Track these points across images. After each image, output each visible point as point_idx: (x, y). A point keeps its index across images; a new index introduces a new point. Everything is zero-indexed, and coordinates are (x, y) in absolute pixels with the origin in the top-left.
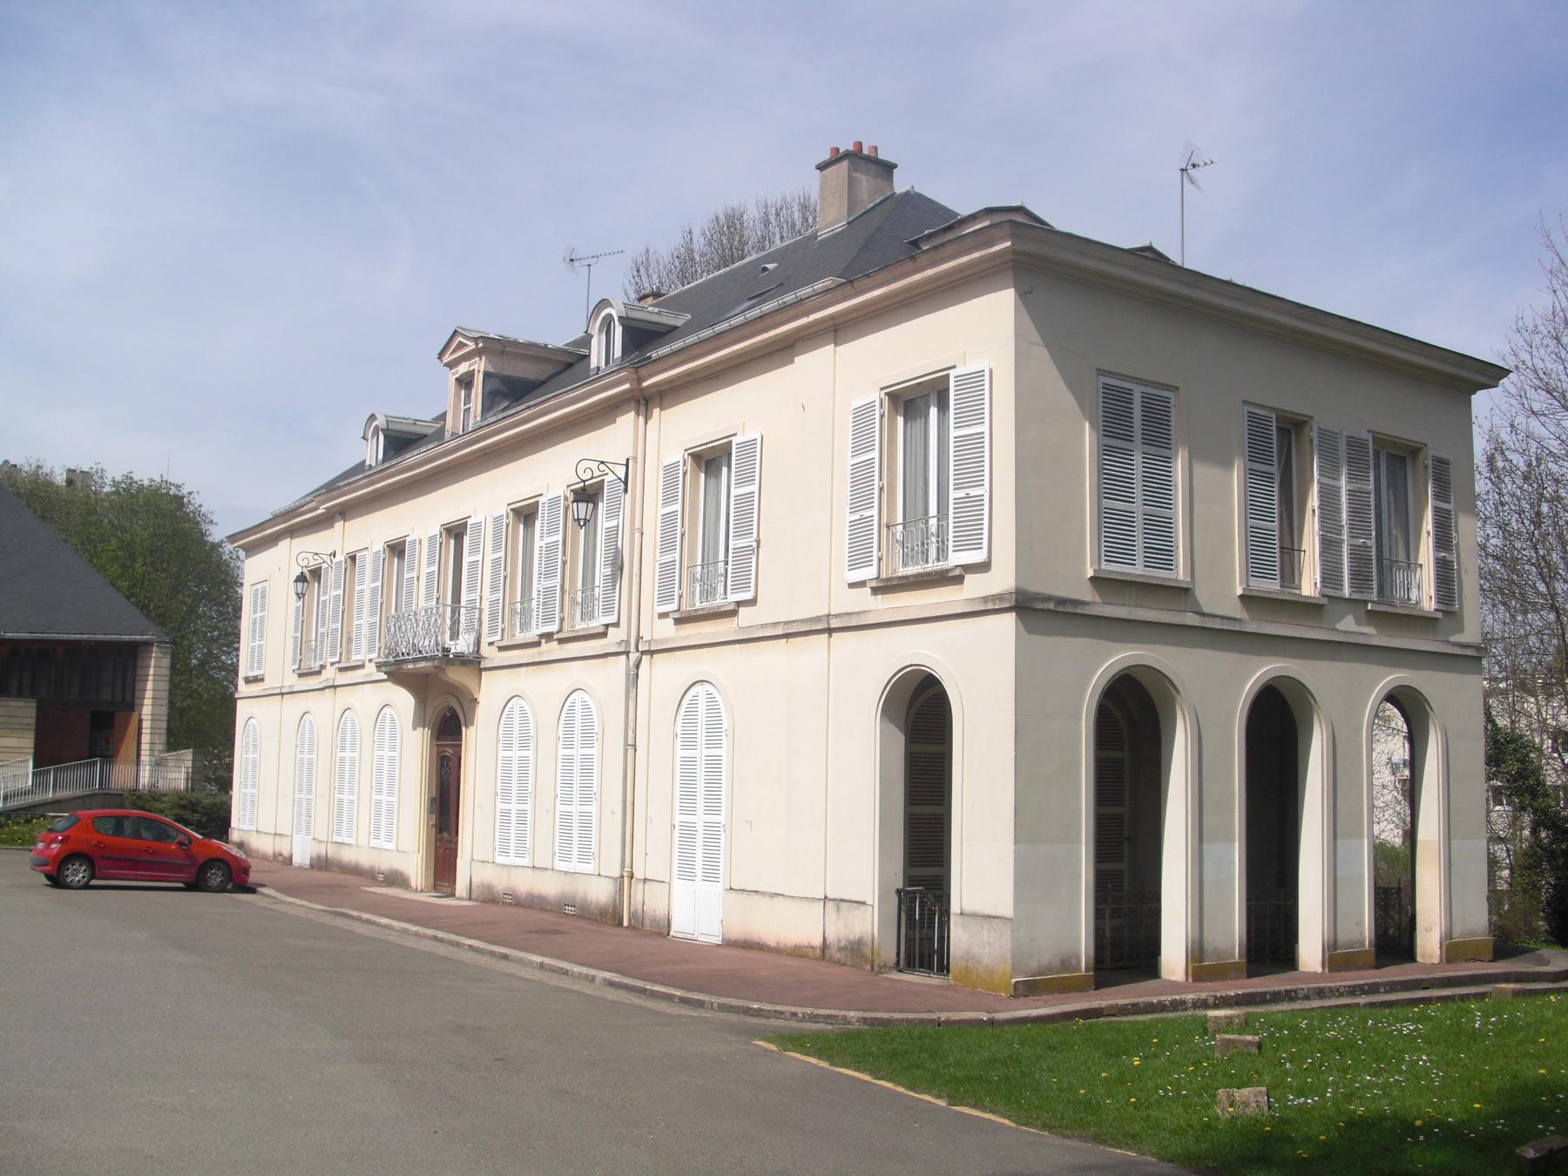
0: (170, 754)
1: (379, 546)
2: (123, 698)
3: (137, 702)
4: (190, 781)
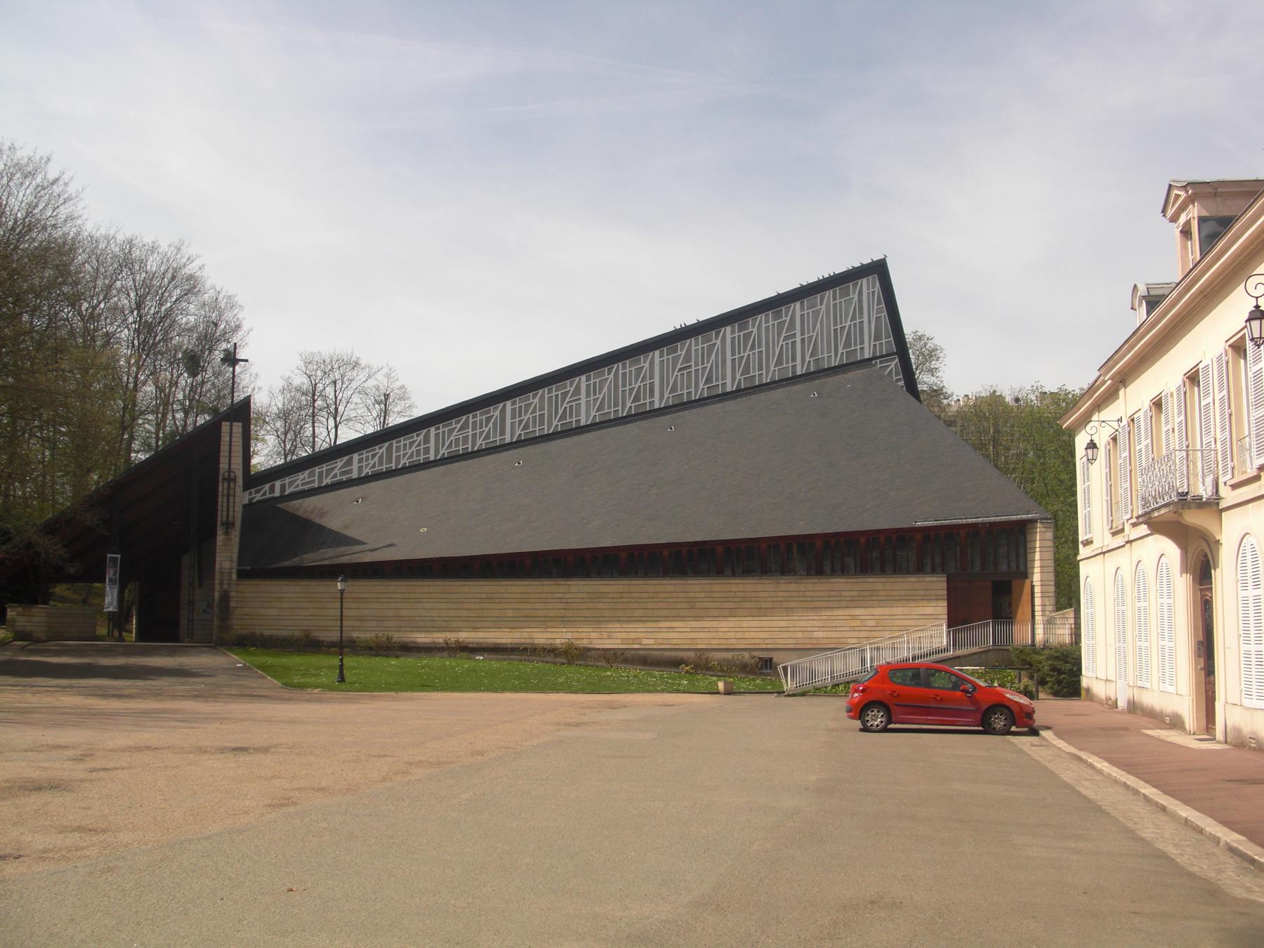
0: (1057, 613)
1: (1146, 404)
2: (1018, 568)
3: (1029, 571)
4: (1074, 636)
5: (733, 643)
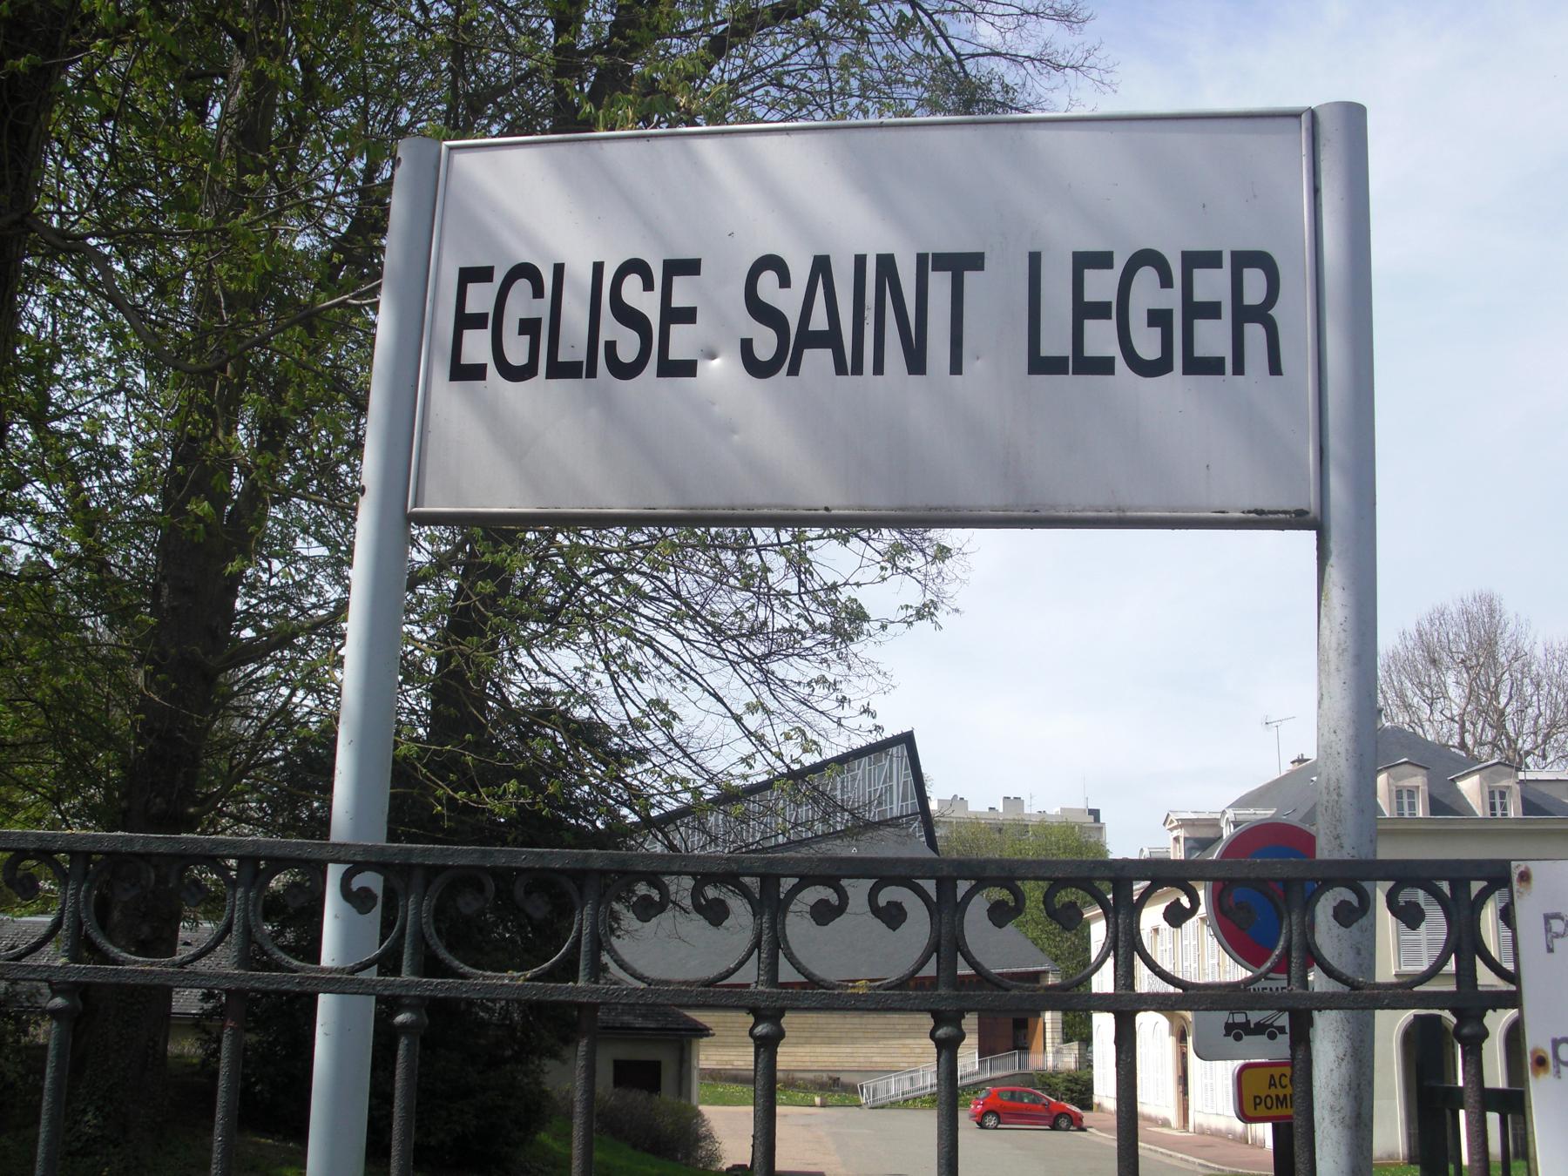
5: (808, 1066)
